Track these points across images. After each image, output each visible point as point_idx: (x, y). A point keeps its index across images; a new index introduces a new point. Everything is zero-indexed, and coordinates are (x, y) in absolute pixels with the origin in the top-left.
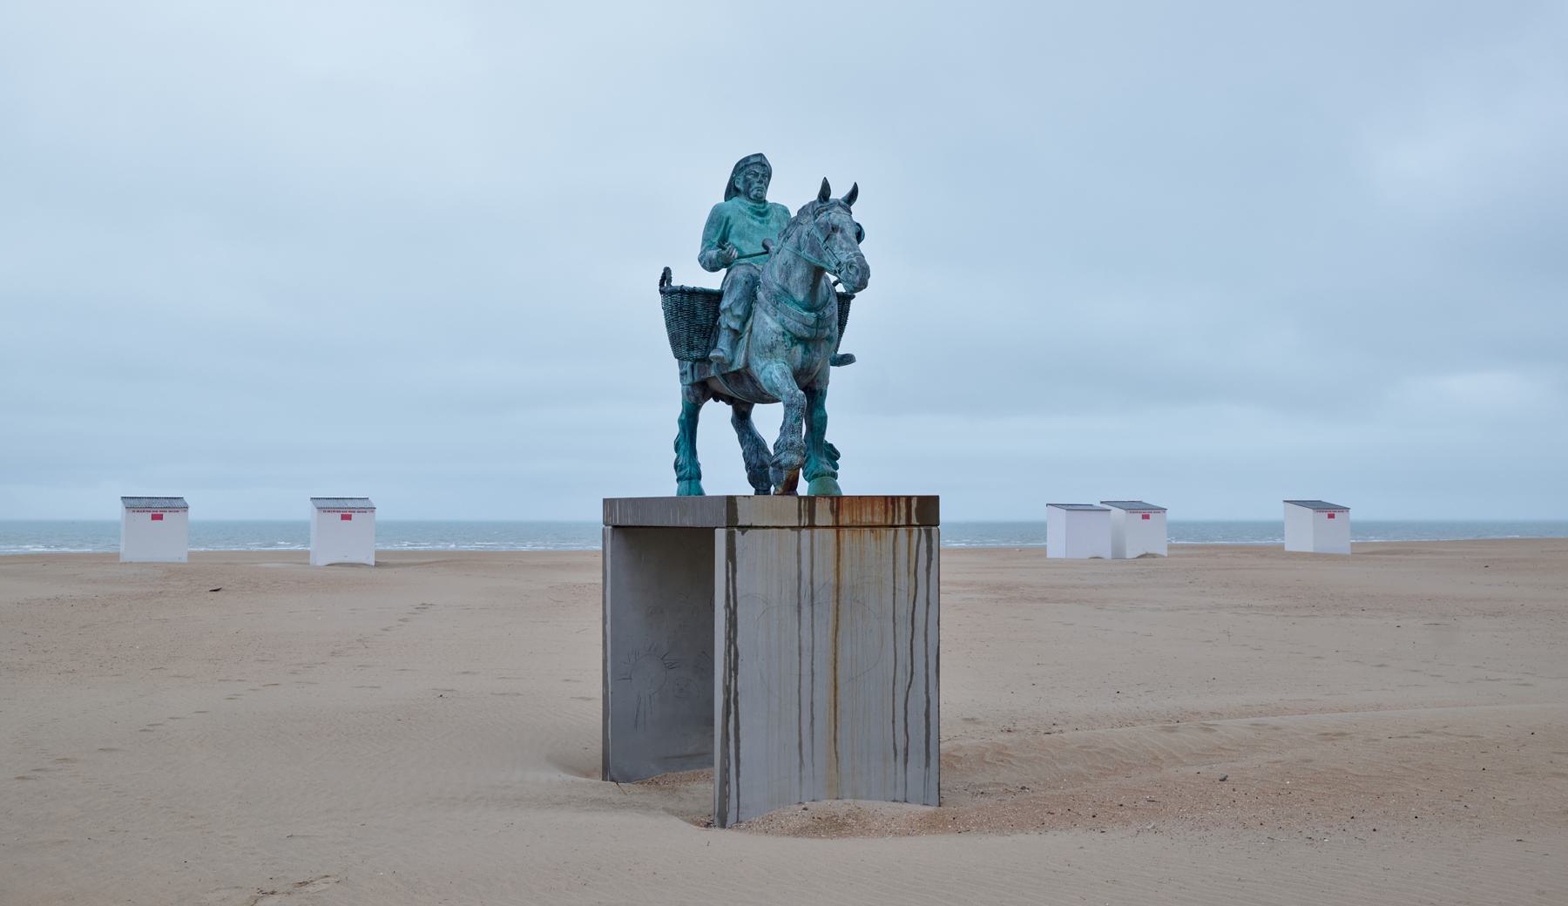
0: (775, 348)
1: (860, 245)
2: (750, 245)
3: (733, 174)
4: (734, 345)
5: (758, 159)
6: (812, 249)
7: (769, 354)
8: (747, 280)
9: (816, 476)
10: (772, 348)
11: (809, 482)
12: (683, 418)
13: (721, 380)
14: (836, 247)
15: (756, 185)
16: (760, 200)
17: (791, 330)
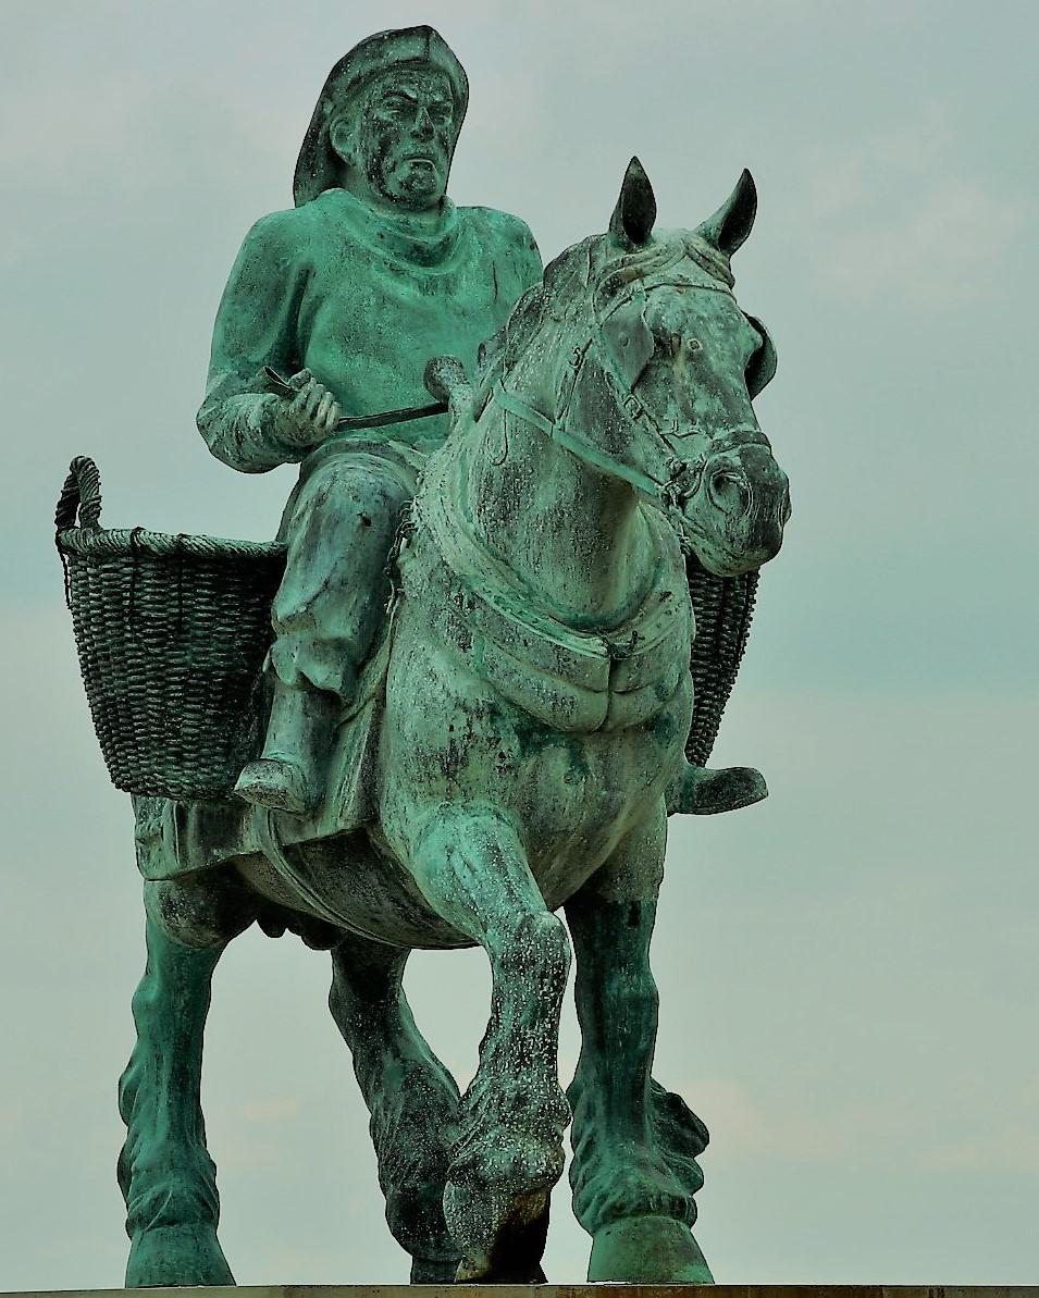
0: (464, 762)
1: (242, 1276)
2: (383, 372)
3: (321, 103)
4: (324, 744)
5: (413, 49)
6: (589, 417)
7: (442, 784)
8: (370, 510)
9: (616, 1212)
10: (452, 763)
11: (592, 1234)
12: (152, 995)
13: (282, 866)
14: (673, 410)
15: (408, 146)
16: (425, 200)
17: (519, 698)
